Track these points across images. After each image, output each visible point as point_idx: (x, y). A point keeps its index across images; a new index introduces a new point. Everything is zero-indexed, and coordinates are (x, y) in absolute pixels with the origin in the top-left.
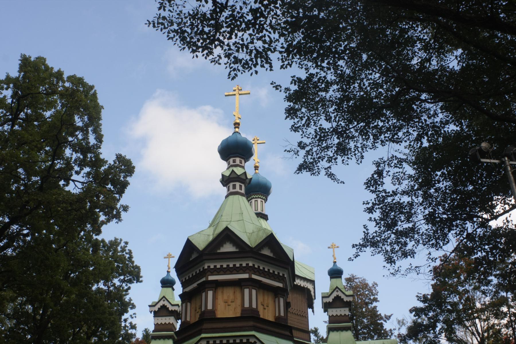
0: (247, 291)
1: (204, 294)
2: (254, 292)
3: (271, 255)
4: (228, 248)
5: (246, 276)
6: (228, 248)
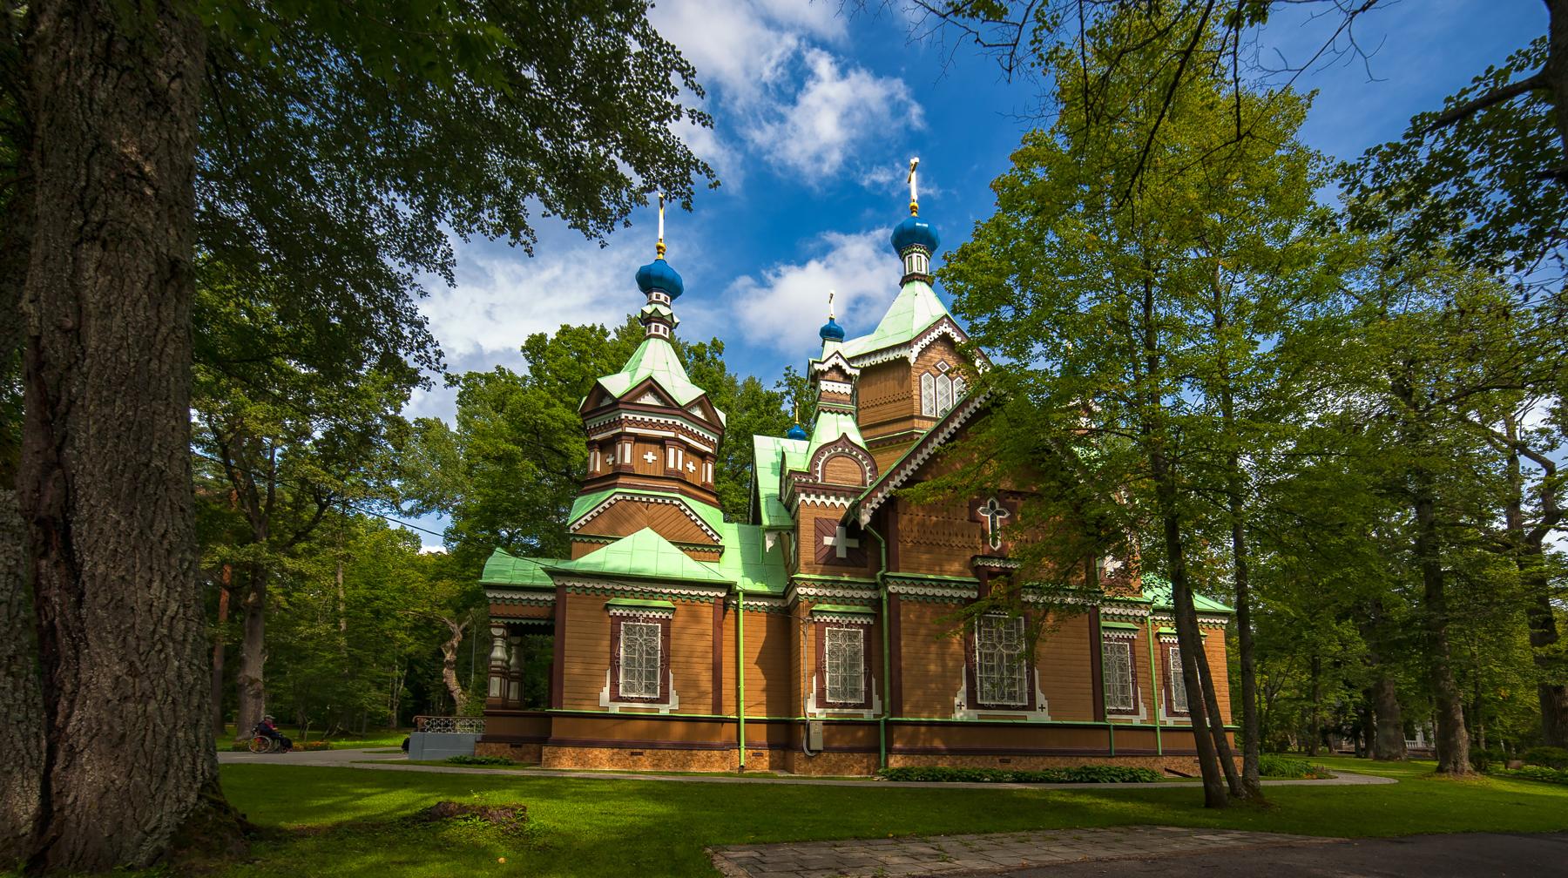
0: (671, 452)
1: (619, 446)
2: (680, 453)
3: (702, 417)
5: (672, 435)
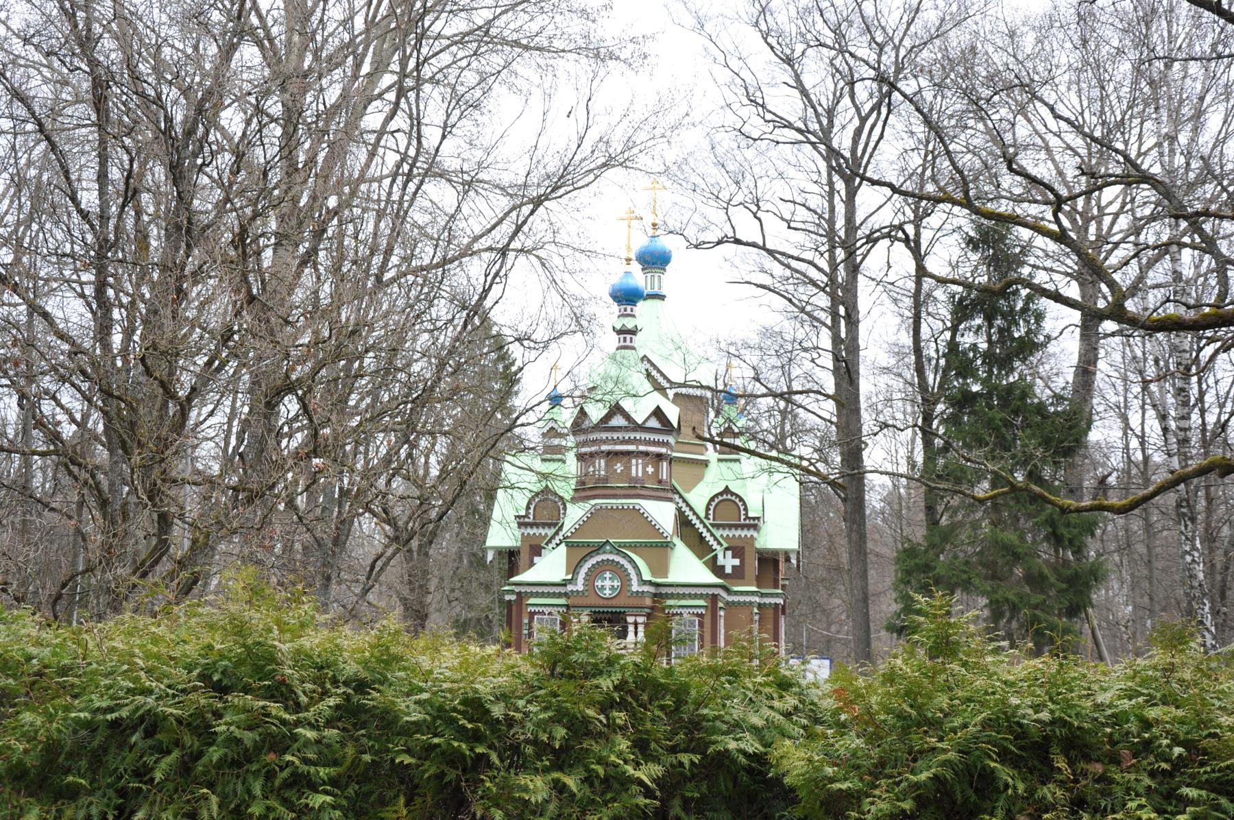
0: (634, 461)
4: (618, 421)
6: (618, 421)
